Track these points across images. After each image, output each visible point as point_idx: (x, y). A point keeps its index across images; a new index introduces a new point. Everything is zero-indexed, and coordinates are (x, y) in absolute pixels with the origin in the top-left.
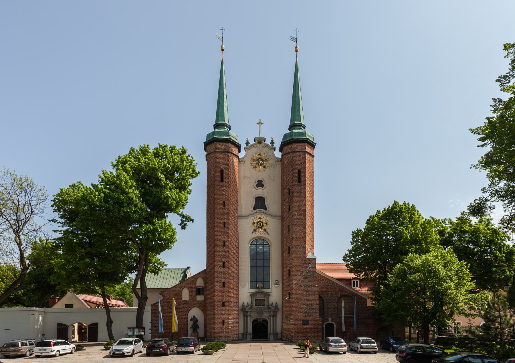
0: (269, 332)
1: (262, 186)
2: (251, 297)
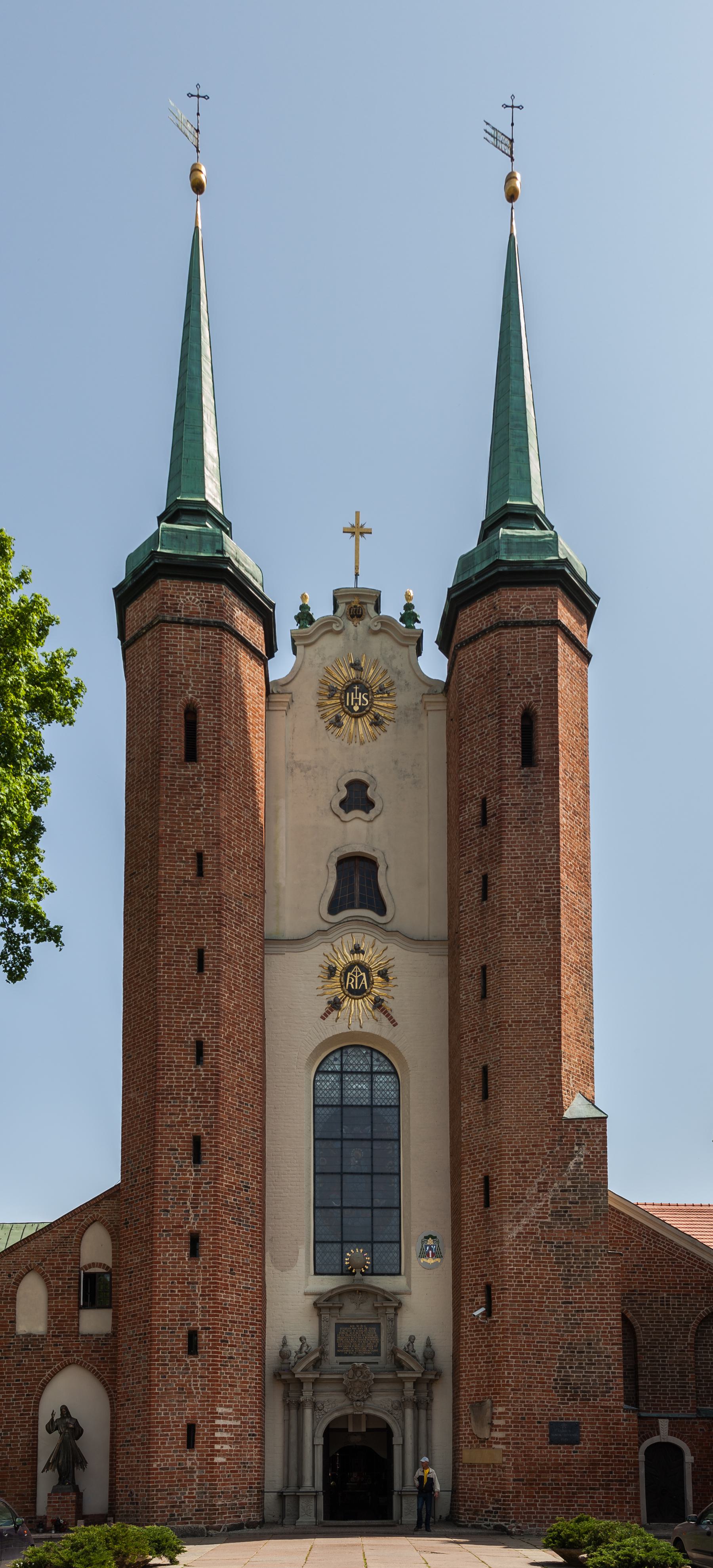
0: (397, 1486)
1: (368, 805)
2: (320, 1316)
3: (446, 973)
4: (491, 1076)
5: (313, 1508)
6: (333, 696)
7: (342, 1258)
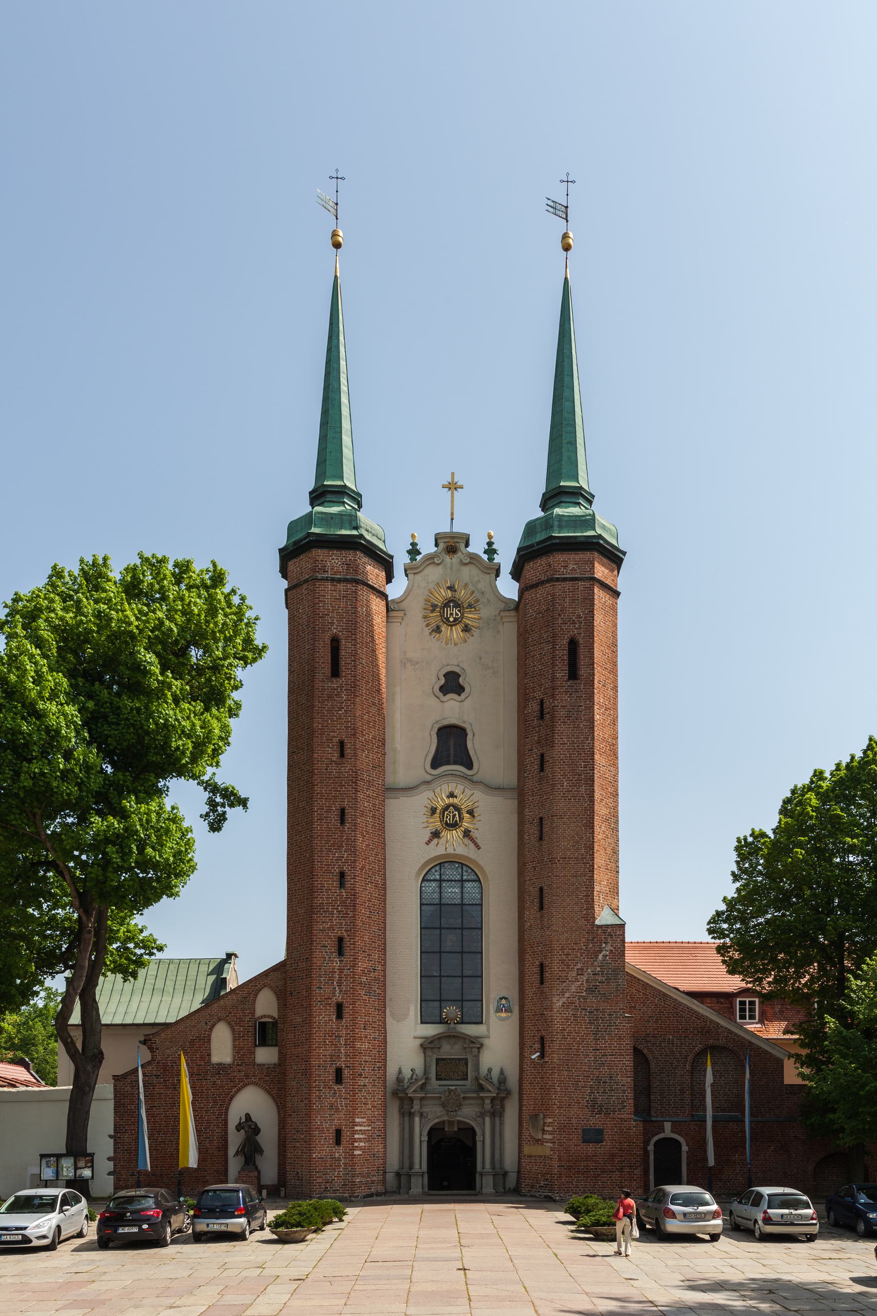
2: (425, 1053)
3: (516, 811)
4: (545, 895)
5: (420, 1183)
6: (434, 610)
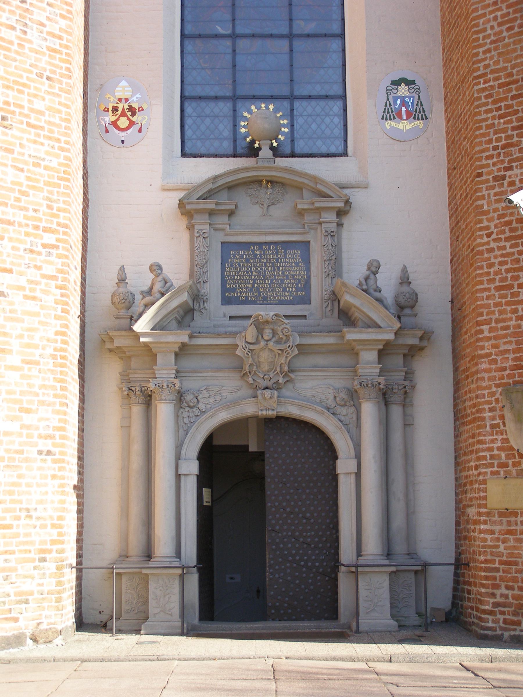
2: (190, 227)
7: (235, 126)
